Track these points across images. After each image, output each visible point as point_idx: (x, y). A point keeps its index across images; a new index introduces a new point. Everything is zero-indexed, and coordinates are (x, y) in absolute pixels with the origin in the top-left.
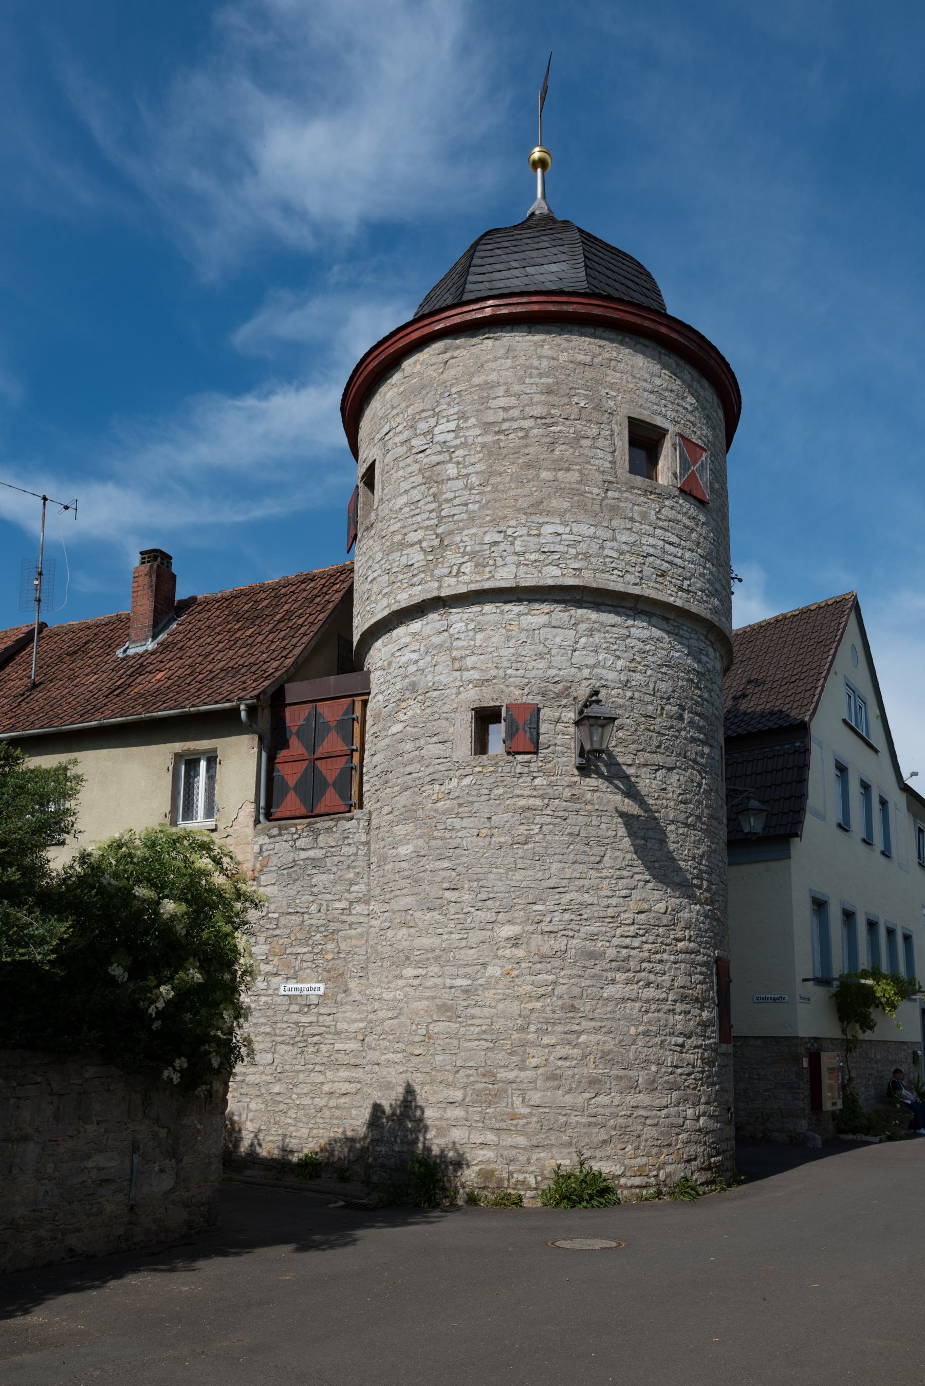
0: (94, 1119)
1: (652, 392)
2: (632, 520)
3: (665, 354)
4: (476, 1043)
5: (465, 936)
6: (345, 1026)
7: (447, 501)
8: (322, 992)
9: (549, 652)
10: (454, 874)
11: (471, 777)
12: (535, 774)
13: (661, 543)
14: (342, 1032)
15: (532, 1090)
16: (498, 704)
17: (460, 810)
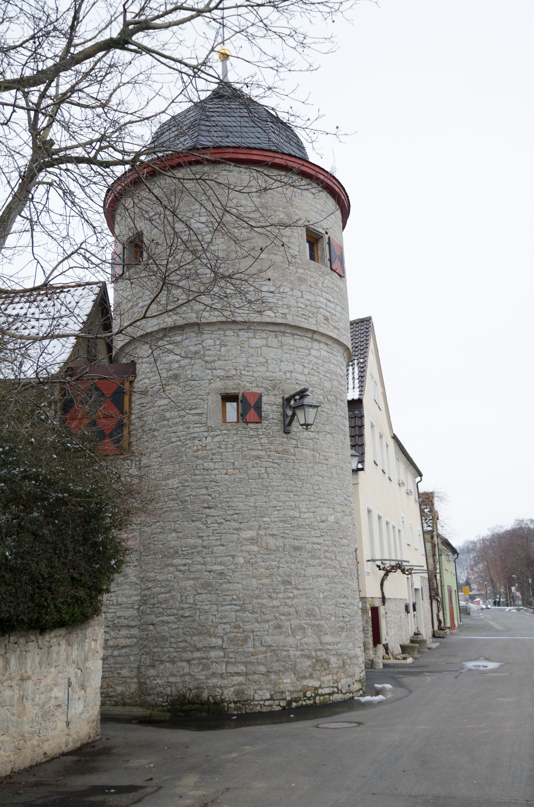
0: (54, 664)
4: (230, 607)
5: (219, 538)
6: (125, 599)
10: (210, 498)
11: (221, 437)
14: (122, 604)
16: (237, 392)
17: (213, 457)
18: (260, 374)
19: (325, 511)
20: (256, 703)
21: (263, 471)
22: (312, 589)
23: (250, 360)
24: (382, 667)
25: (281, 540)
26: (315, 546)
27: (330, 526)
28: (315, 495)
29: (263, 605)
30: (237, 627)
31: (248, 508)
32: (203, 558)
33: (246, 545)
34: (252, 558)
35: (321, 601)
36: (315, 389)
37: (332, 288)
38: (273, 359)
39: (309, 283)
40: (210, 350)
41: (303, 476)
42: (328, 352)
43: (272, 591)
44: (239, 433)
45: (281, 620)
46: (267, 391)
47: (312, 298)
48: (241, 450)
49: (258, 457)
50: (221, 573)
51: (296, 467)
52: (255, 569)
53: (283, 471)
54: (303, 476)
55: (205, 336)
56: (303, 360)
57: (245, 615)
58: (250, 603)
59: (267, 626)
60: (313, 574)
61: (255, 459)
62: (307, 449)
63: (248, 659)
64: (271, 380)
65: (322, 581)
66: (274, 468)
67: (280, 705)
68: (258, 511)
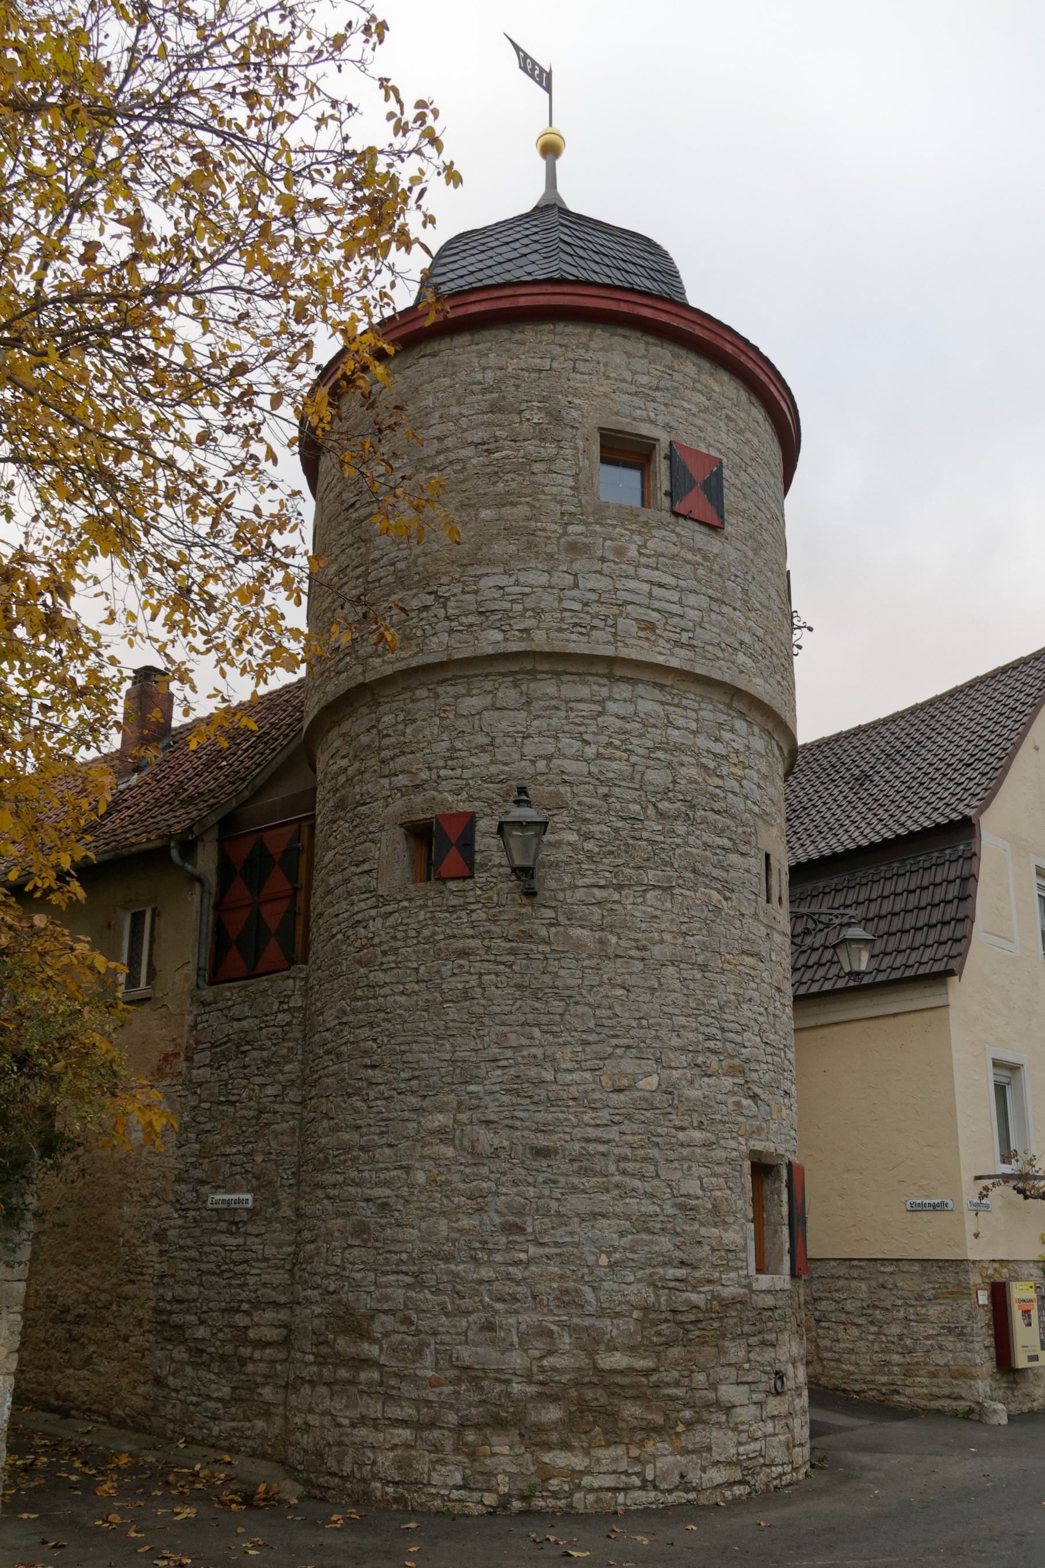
1: (636, 394)
2: (603, 559)
3: (655, 345)
6: (274, 1251)
7: (375, 561)
8: (250, 1205)
9: (492, 744)
12: (473, 907)
13: (646, 587)
15: (460, 1344)
16: (429, 816)
17: (385, 959)
18: (477, 770)
19: (629, 1065)
20: (433, 1491)
21: (473, 983)
22: (577, 1245)
23: (458, 744)
24: (1004, 1421)
25: (504, 1133)
26: (591, 1147)
27: (645, 1100)
28: (599, 1030)
29: (457, 1275)
30: (407, 1321)
31: (438, 1064)
32: (360, 1171)
33: (430, 1144)
34: (441, 1173)
35: (600, 1272)
36: (617, 791)
37: (674, 557)
38: (507, 734)
39: (599, 553)
40: (388, 735)
41: (567, 988)
42: (662, 703)
43: (477, 1245)
44: (430, 903)
45: (496, 1312)
46: (490, 806)
47: (604, 583)
48: (431, 940)
49: (464, 953)
50: (384, 1206)
51: (550, 969)
52: (447, 1197)
53: (517, 979)
54: (567, 988)
55: (383, 709)
56: (582, 729)
57: (420, 1296)
58: (432, 1272)
59: (464, 1324)
60: (582, 1210)
61: (459, 957)
62: (582, 927)
63: (423, 1394)
64: (500, 782)
65: (606, 1230)
66: (497, 974)
67: (481, 1502)
68: (458, 1071)
